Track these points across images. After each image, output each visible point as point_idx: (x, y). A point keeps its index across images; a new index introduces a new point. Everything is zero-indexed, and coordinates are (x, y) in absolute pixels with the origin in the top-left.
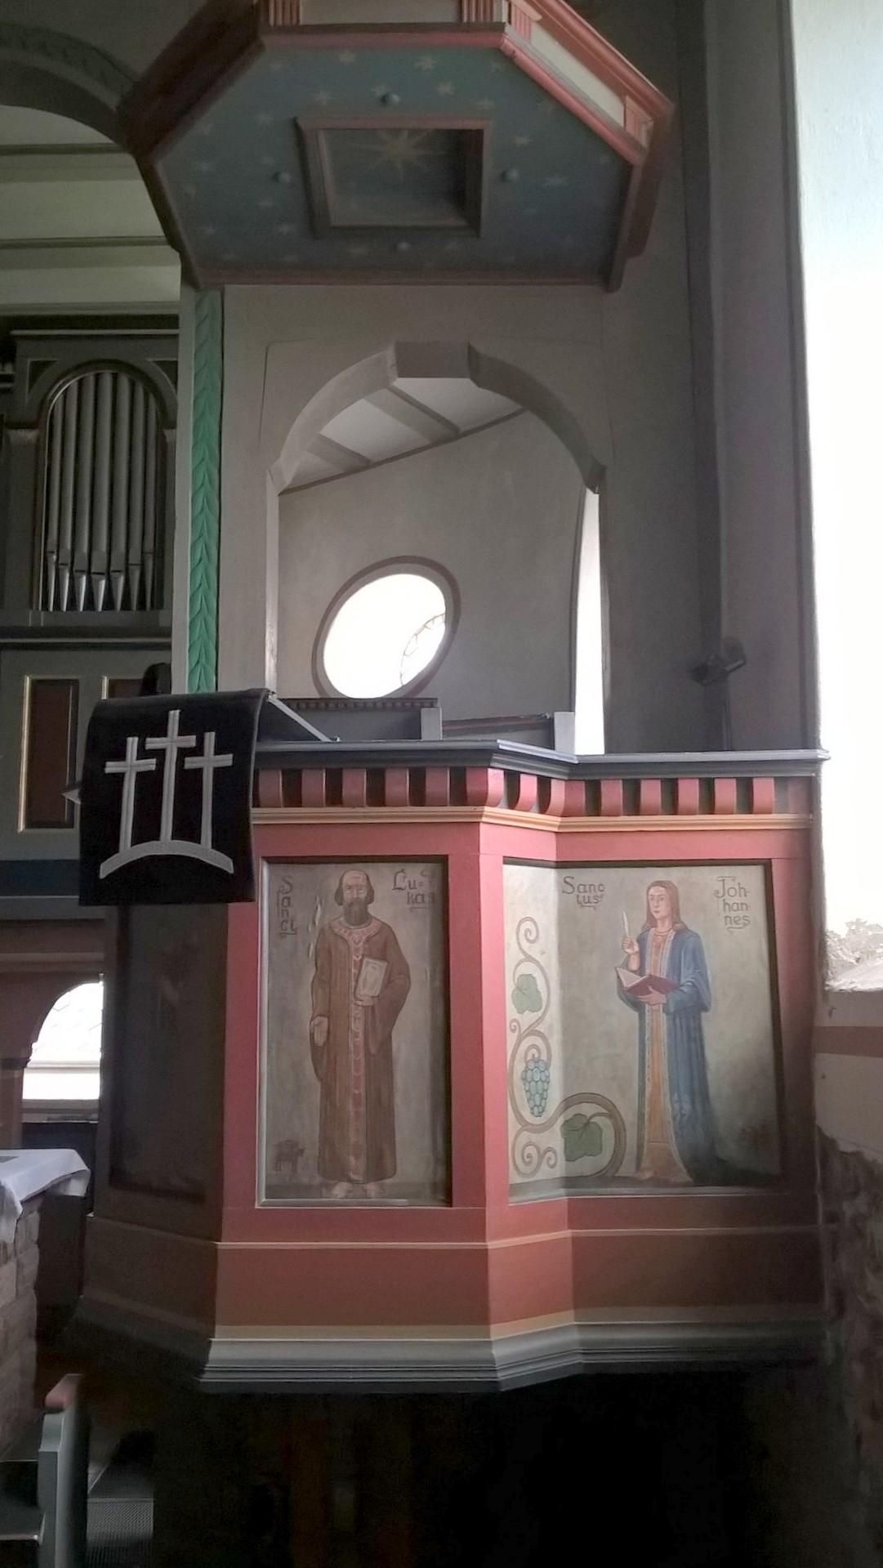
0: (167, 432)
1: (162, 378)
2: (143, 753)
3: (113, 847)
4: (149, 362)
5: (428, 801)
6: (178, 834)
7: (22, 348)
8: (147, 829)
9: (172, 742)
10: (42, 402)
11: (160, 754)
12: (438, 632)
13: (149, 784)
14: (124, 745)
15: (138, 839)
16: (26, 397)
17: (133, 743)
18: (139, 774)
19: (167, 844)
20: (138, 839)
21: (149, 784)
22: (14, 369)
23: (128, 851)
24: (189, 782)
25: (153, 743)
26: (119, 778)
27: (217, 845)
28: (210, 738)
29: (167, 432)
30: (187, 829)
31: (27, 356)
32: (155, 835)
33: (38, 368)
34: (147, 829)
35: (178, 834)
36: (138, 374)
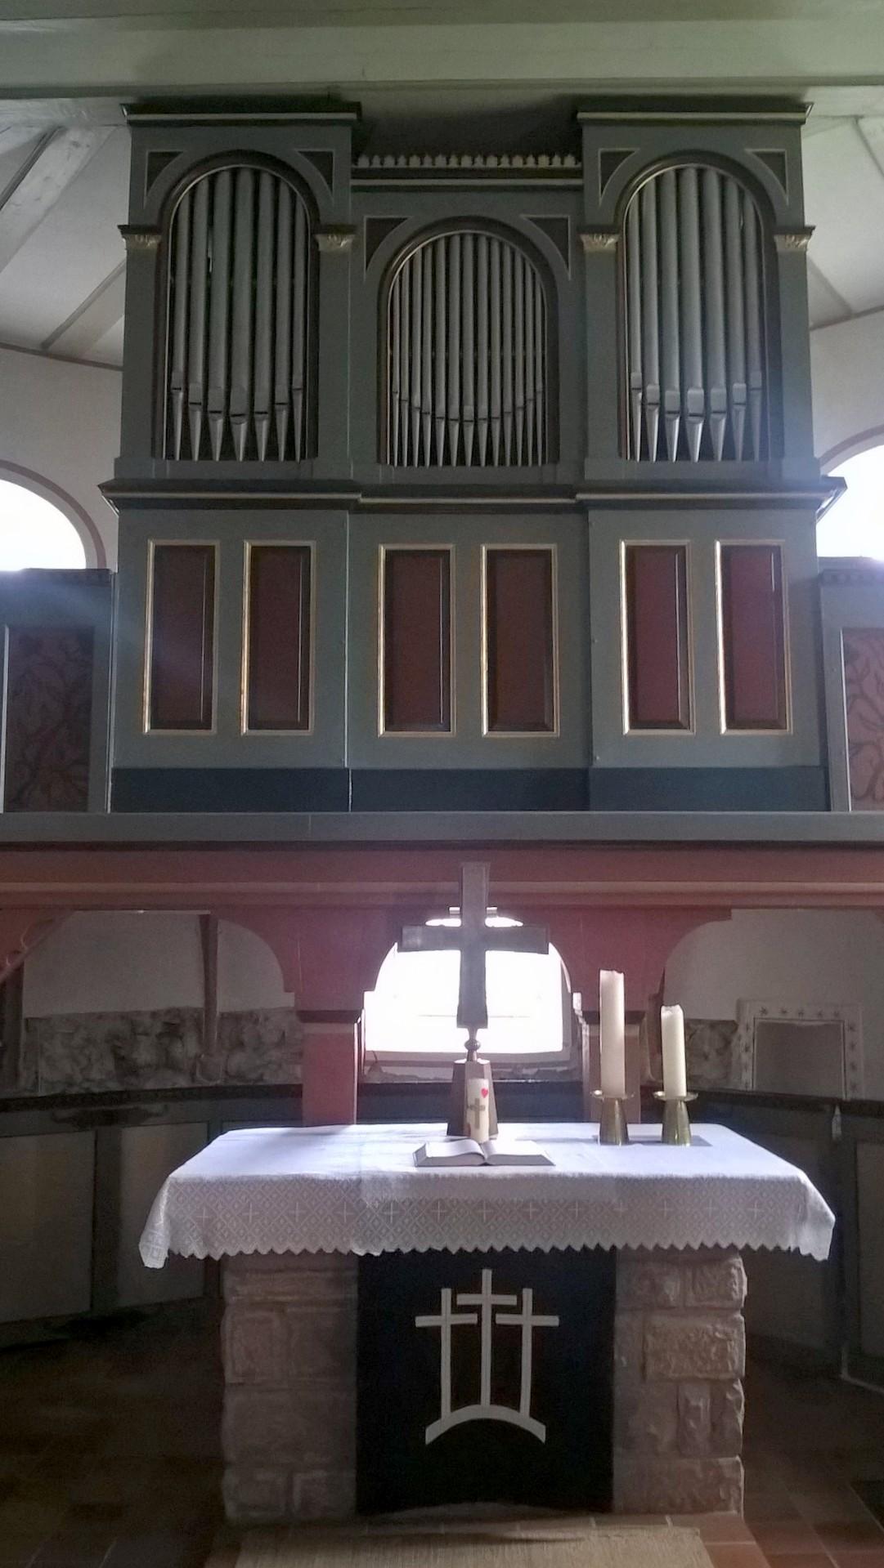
0: (784, 244)
1: (766, 175)
2: (457, 1309)
3: (436, 1415)
4: (748, 154)
5: (618, 1502)
6: (496, 1399)
7: (588, 133)
8: (465, 1394)
9: (486, 1298)
10: (626, 187)
11: (476, 1309)
12: (143, 1252)
13: (466, 1338)
14: (424, 1329)
15: (456, 1404)
16: (600, 200)
17: (446, 1294)
18: (453, 1327)
19: (485, 1409)
20: (456, 1404)
21: (466, 1338)
22: (579, 159)
23: (449, 1417)
24: (507, 1338)
25: (464, 1299)
26: (437, 1330)
27: (534, 1414)
28: (528, 1294)
29: (784, 244)
30: (506, 1394)
31: (596, 144)
32: (475, 1399)
33: (611, 161)
34: (465, 1394)
35: (496, 1399)
36: (734, 168)
